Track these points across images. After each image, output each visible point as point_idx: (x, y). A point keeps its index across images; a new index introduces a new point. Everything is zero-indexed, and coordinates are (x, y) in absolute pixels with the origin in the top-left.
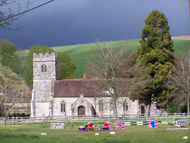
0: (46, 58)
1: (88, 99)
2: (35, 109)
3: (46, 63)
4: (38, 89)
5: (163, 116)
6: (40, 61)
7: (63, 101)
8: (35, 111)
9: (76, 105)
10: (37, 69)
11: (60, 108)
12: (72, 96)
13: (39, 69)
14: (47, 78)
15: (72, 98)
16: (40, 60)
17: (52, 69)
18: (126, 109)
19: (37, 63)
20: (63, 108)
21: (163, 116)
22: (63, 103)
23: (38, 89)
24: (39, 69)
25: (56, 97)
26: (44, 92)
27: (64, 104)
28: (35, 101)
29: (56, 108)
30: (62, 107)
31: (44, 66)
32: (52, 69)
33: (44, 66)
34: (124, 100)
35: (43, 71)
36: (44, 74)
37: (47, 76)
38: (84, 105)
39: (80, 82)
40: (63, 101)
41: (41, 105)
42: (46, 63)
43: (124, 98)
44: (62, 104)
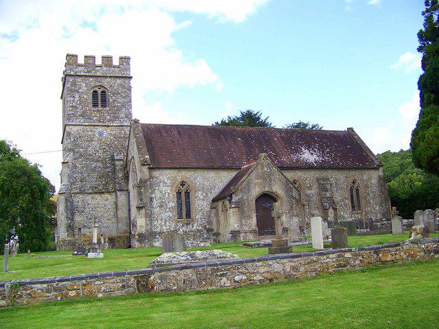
0: (105, 69)
2: (73, 214)
4: (81, 155)
6: (87, 74)
8: (72, 219)
9: (249, 189)
10: (77, 96)
12: (175, 165)
13: (85, 96)
14: (107, 124)
15: (211, 175)
16: (88, 72)
17: (121, 100)
22: (183, 189)
23: (81, 155)
24: (85, 96)
26: (99, 164)
27: (187, 194)
28: (71, 190)
31: (99, 91)
32: (121, 100)
33: (99, 91)
34: (351, 180)
35: (95, 105)
36: (98, 111)
37: (108, 117)
38: (278, 189)
40: (183, 184)
41: (89, 202)
42: (105, 82)
43: (352, 173)
44: (179, 193)
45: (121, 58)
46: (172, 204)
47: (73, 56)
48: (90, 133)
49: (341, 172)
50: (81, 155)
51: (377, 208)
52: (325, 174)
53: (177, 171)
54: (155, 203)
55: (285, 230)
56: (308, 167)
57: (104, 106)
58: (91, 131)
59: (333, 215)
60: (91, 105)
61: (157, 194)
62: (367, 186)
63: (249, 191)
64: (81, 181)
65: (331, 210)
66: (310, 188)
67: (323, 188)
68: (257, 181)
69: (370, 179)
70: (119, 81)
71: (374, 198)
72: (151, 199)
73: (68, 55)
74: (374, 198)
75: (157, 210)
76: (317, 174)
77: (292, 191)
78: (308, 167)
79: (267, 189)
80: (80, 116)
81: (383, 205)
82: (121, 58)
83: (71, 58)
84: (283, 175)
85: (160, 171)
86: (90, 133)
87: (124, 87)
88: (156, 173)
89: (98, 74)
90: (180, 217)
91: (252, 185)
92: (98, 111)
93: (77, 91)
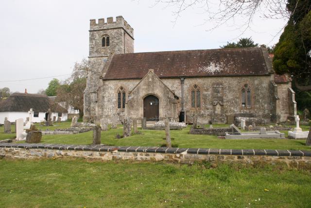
0: (108, 25)
1: (168, 83)
3: (108, 32)
5: (219, 125)
7: (122, 88)
8: (89, 106)
10: (94, 42)
11: (115, 100)
17: (116, 41)
18: (122, 105)
19: (95, 32)
20: (122, 101)
21: (219, 125)
22: (196, 90)
23: (95, 73)
25: (109, 80)
29: (108, 101)
30: (119, 99)
32: (116, 41)
34: (243, 84)
35: (103, 45)
38: (158, 92)
39: (292, 88)
40: (122, 88)
42: (108, 32)
44: (119, 94)
45: (117, 17)
46: (114, 100)
47: (110, 18)
48: (100, 61)
49: (234, 78)
50: (95, 73)
51: (266, 106)
52: (220, 80)
53: (118, 81)
54: (106, 99)
55: (284, 117)
56: (208, 76)
57: (108, 45)
58: (100, 59)
59: (220, 109)
60: (101, 46)
61: (107, 94)
62: (257, 89)
63: (138, 93)
64: (95, 86)
65: (218, 107)
66: (207, 90)
67: (216, 91)
68: (144, 87)
69: (261, 83)
70: (115, 31)
71: (263, 98)
72: (103, 97)
73: (90, 20)
74: (263, 98)
75: (106, 103)
76: (214, 80)
77: (168, 93)
78: (208, 76)
79: (150, 92)
80: (96, 52)
81: (271, 103)
82: (117, 17)
83: (93, 22)
84: (162, 83)
85: (109, 81)
86: (100, 61)
87: (118, 33)
88: (107, 83)
89: (105, 28)
90: (119, 107)
91: (141, 90)
92: (104, 48)
93: (94, 39)
